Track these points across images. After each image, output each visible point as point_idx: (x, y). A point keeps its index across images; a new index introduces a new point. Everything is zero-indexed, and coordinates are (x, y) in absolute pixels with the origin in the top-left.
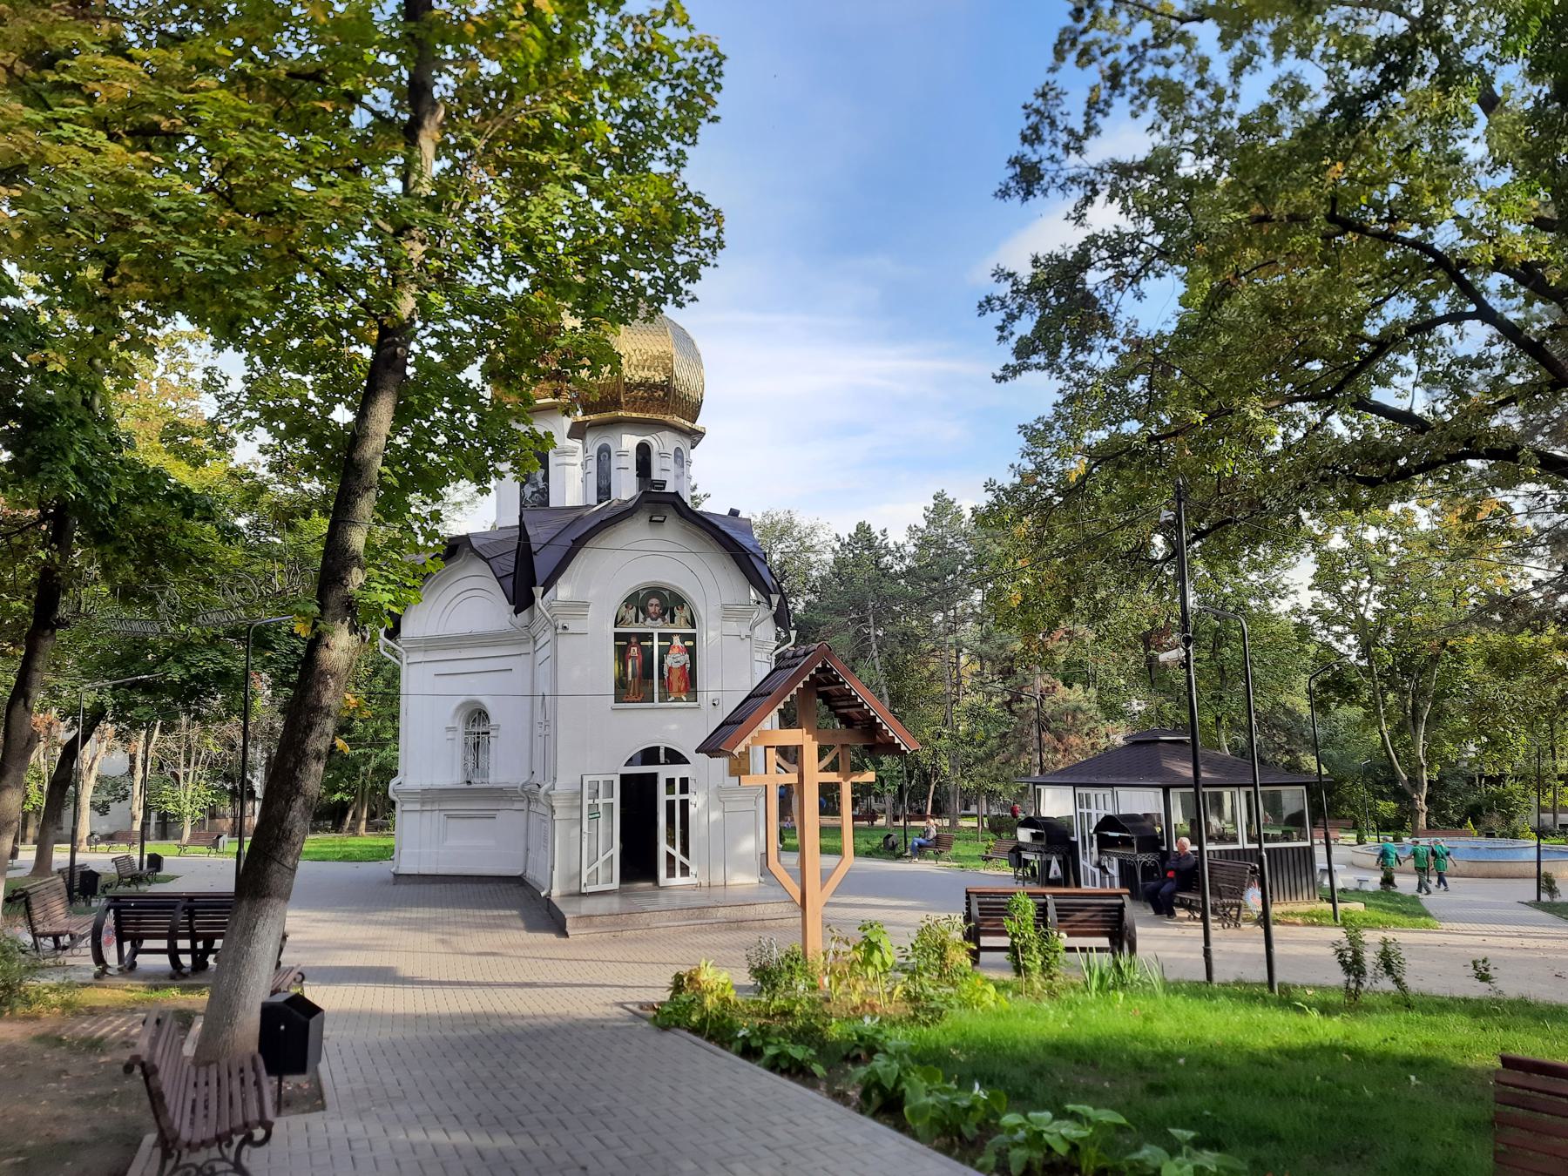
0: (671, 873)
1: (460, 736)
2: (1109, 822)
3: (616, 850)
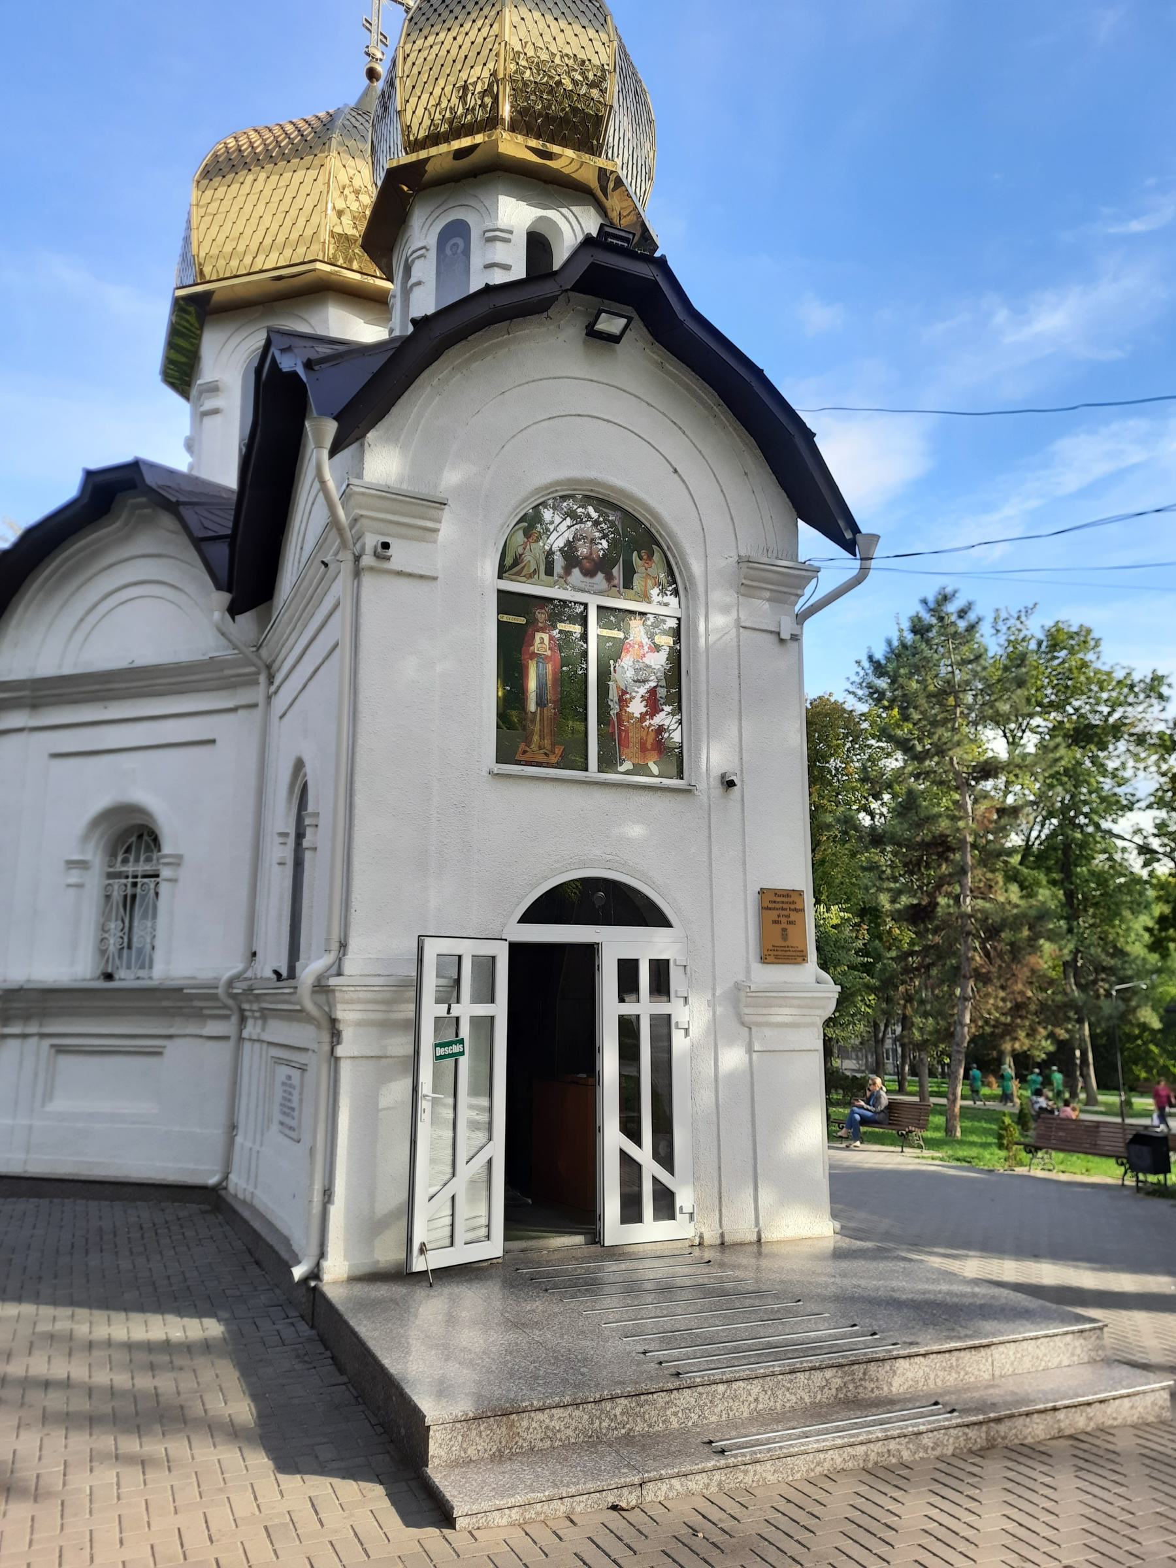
0: (631, 1212)
1: (94, 880)
3: (497, 1150)
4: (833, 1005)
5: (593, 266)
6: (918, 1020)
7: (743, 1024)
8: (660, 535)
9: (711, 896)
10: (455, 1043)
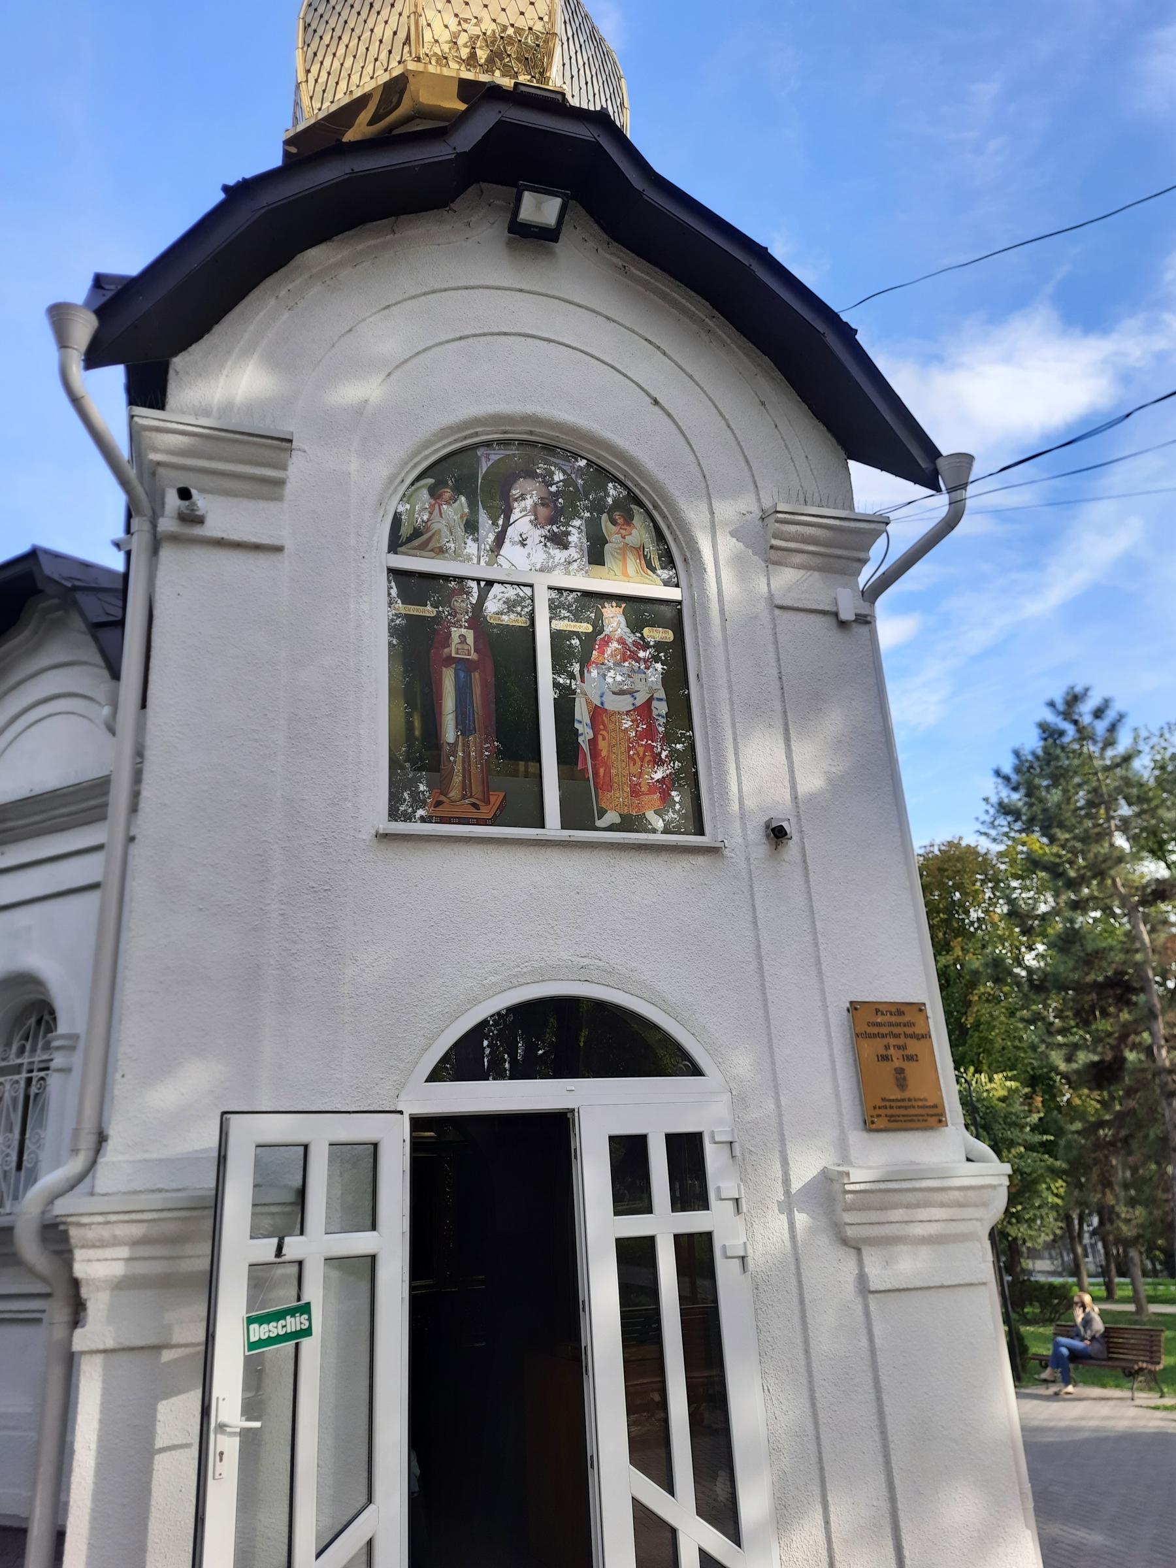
4: (1001, 1200)
5: (500, 123)
6: (1123, 1210)
7: (845, 1242)
8: (641, 489)
9: (767, 1019)
10: (292, 1312)
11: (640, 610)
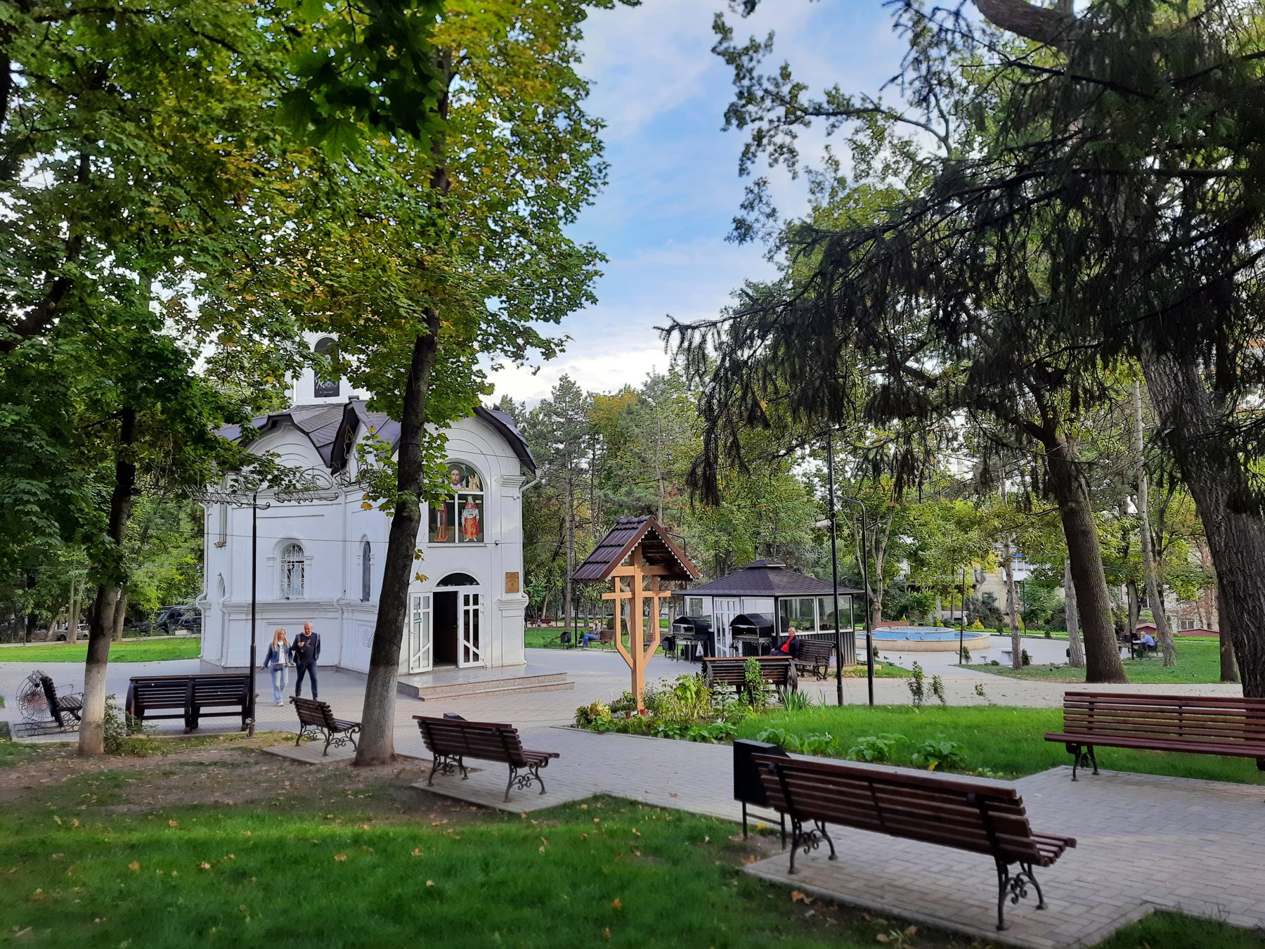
1: (278, 564)
2: (741, 619)
3: (431, 645)
11: (475, 497)
